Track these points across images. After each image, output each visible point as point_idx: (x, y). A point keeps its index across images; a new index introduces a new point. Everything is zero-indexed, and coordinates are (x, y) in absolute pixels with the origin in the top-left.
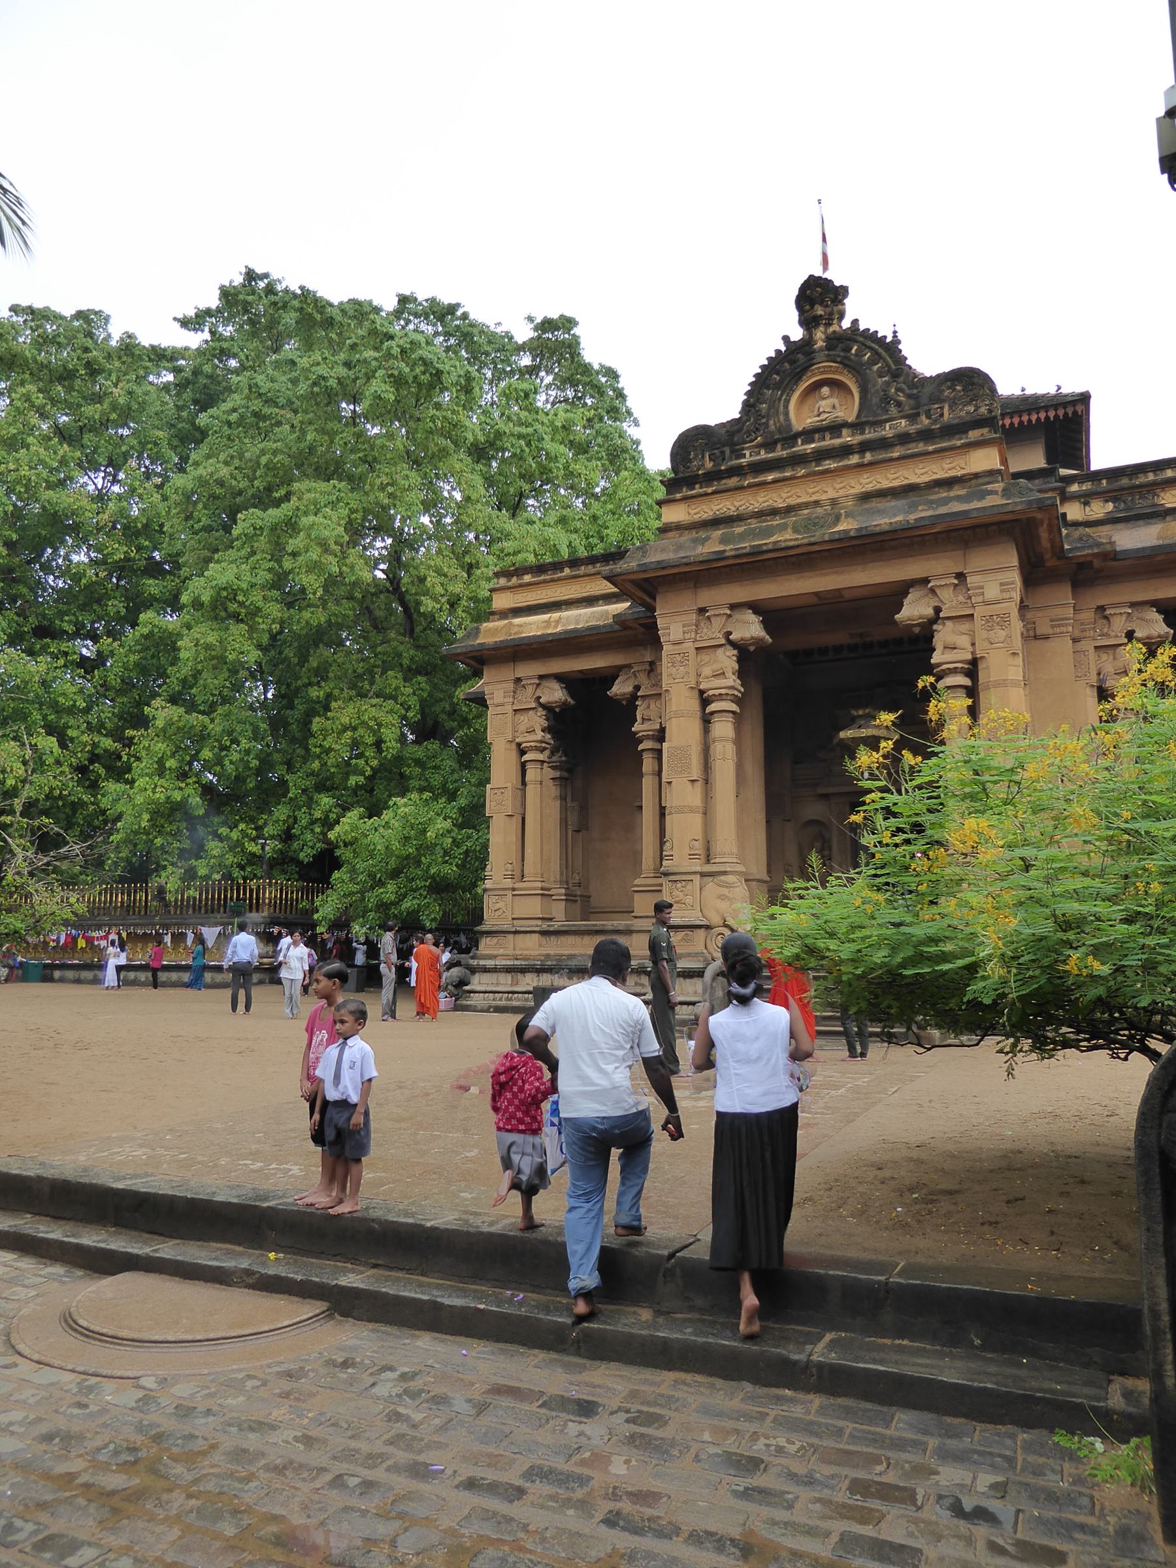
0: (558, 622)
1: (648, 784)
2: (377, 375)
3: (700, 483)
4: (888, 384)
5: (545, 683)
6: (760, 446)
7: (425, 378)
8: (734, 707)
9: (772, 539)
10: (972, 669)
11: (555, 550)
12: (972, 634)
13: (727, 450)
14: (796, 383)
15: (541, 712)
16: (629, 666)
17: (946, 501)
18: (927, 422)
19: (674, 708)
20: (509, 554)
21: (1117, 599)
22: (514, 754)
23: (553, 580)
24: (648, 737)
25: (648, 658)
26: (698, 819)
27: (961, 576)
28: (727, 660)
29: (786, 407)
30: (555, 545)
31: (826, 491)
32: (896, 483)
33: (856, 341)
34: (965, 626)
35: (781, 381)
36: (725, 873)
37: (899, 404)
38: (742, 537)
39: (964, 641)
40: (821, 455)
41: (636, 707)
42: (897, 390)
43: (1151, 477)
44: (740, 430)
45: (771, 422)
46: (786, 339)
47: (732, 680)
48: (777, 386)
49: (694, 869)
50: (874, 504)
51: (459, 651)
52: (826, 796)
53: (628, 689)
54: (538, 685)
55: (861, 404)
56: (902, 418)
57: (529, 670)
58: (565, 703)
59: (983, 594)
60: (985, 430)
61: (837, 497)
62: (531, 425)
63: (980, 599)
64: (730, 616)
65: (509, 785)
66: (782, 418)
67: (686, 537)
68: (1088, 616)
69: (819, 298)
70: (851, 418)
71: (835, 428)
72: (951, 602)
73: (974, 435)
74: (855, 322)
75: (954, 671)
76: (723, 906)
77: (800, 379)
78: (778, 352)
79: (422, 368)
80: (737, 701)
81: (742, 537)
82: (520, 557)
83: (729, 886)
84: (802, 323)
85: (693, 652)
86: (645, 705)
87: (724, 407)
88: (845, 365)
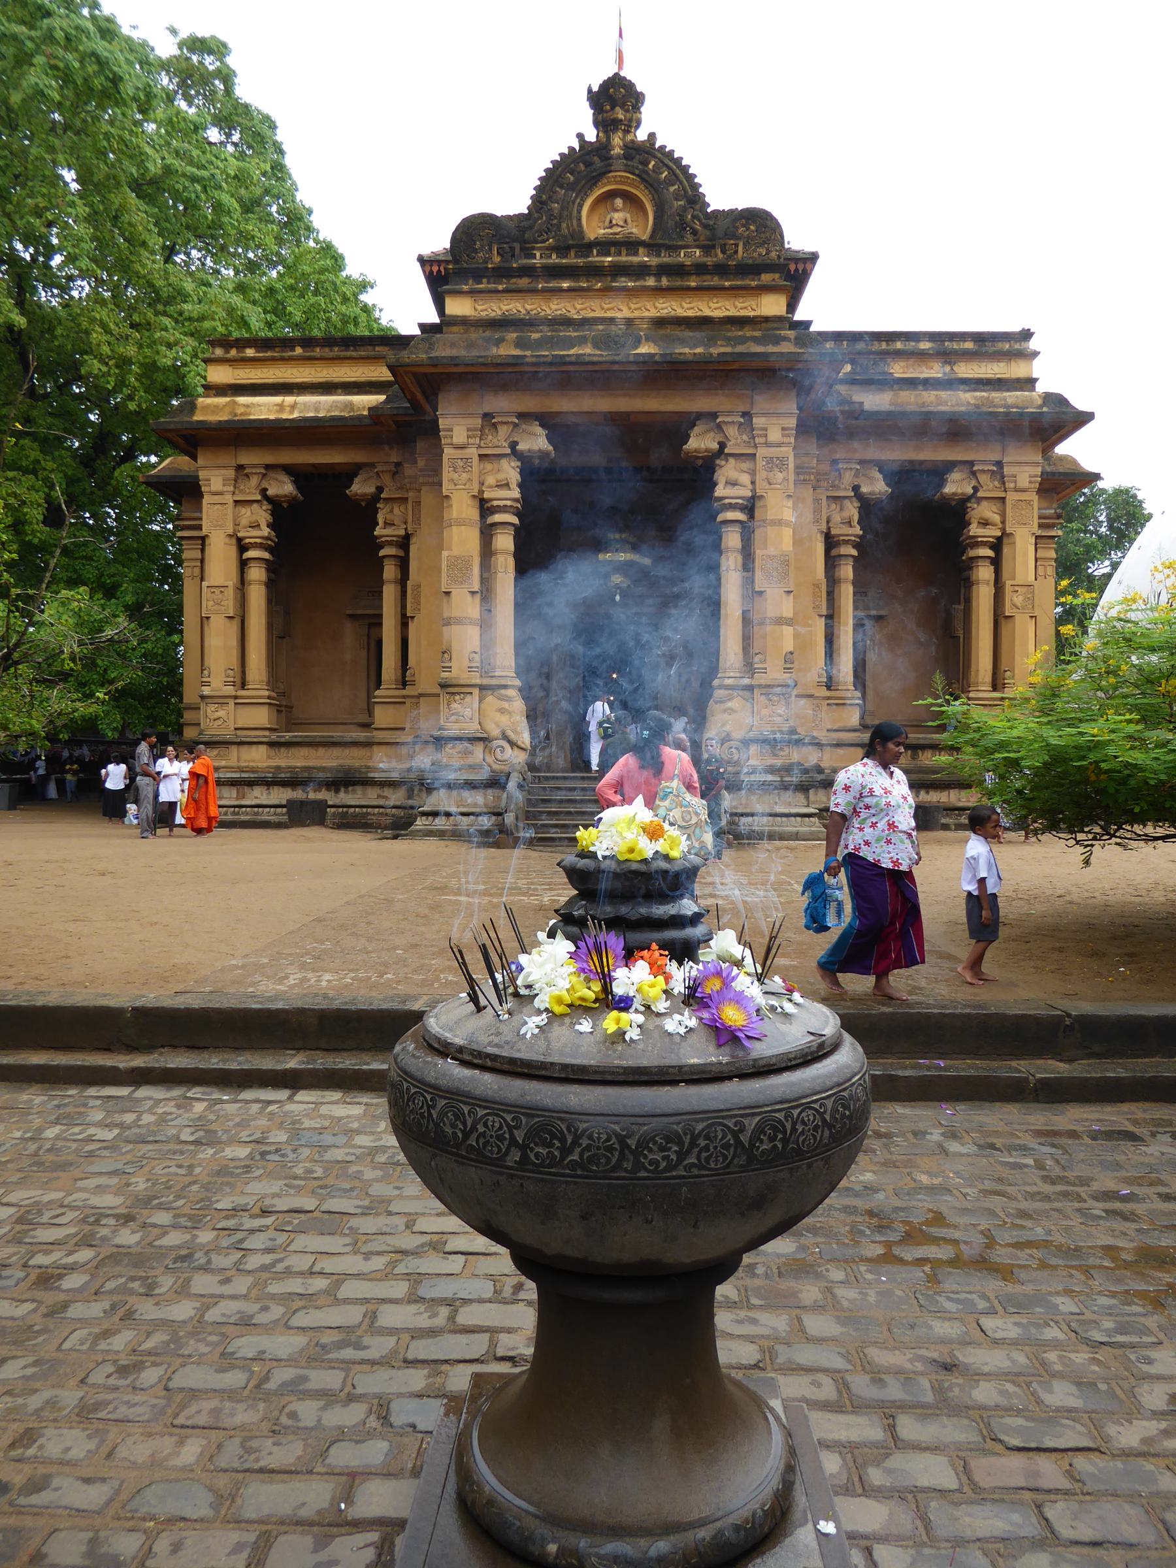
0: (293, 407)
1: (389, 593)
2: (35, 61)
3: (488, 277)
4: (684, 209)
5: (272, 474)
6: (552, 249)
7: (98, 83)
8: (266, 555)
9: (572, 352)
10: (750, 507)
11: (244, 323)
12: (1003, 516)
13: (517, 246)
14: (591, 189)
15: (266, 506)
16: (372, 465)
17: (744, 340)
18: (721, 256)
20: (190, 319)
22: (233, 551)
23: (283, 359)
24: (390, 543)
28: (511, 471)
29: (579, 212)
30: (242, 317)
31: (621, 309)
32: (690, 313)
33: (654, 157)
34: (746, 465)
35: (576, 183)
36: (505, 687)
37: (695, 232)
38: (539, 344)
39: (745, 479)
40: (618, 270)
41: (376, 511)
42: (693, 217)
43: (884, 346)
44: (531, 227)
45: (564, 225)
46: (580, 136)
47: (516, 493)
48: (571, 187)
49: (474, 682)
50: (668, 330)
51: (172, 426)
53: (370, 489)
54: (264, 475)
55: (655, 224)
56: (698, 247)
57: (252, 458)
58: (295, 498)
60: (777, 276)
61: (629, 315)
62: (204, 167)
63: (762, 440)
64: (516, 425)
65: (230, 584)
66: (575, 223)
67: (475, 335)
68: (825, 467)
69: (615, 100)
70: (645, 237)
71: (632, 245)
73: (766, 278)
74: (652, 136)
76: (504, 720)
77: (595, 183)
78: (571, 149)
79: (95, 67)
80: (518, 514)
81: (539, 344)
82: (207, 324)
83: (509, 699)
84: (596, 124)
87: (512, 198)
88: (643, 180)
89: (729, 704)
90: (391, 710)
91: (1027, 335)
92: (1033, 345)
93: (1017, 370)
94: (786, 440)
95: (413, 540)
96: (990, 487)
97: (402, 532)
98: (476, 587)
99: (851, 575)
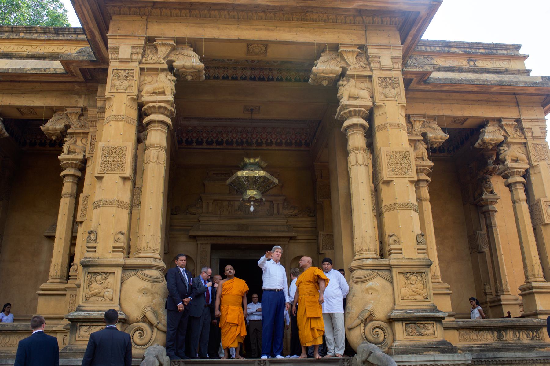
1: (65, 204)
8: (429, 179)
16: (62, 109)
19: (114, 113)
21: (417, 112)
25: (82, 103)
26: (125, 214)
27: (363, 48)
28: (166, 83)
34: (367, 84)
39: (365, 94)
52: (194, 238)
53: (60, 126)
54: (173, 49)
59: (379, 62)
63: (377, 65)
72: (354, 65)
75: (356, 114)
80: (170, 116)
85: (137, 72)
86: (72, 141)
89: (370, 284)
90: (53, 301)
91: (518, 47)
92: (522, 52)
93: (514, 65)
94: (396, 66)
95: (89, 163)
96: (514, 136)
97: (81, 157)
98: (128, 173)
99: (428, 196)
